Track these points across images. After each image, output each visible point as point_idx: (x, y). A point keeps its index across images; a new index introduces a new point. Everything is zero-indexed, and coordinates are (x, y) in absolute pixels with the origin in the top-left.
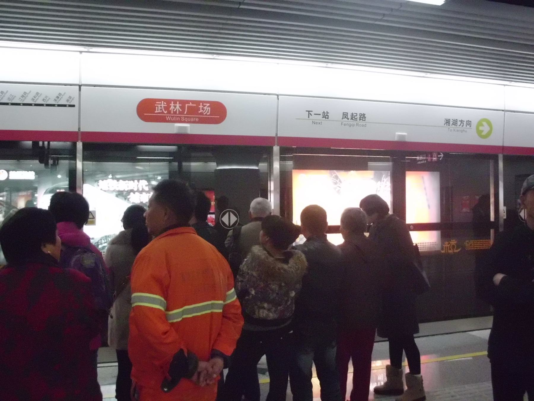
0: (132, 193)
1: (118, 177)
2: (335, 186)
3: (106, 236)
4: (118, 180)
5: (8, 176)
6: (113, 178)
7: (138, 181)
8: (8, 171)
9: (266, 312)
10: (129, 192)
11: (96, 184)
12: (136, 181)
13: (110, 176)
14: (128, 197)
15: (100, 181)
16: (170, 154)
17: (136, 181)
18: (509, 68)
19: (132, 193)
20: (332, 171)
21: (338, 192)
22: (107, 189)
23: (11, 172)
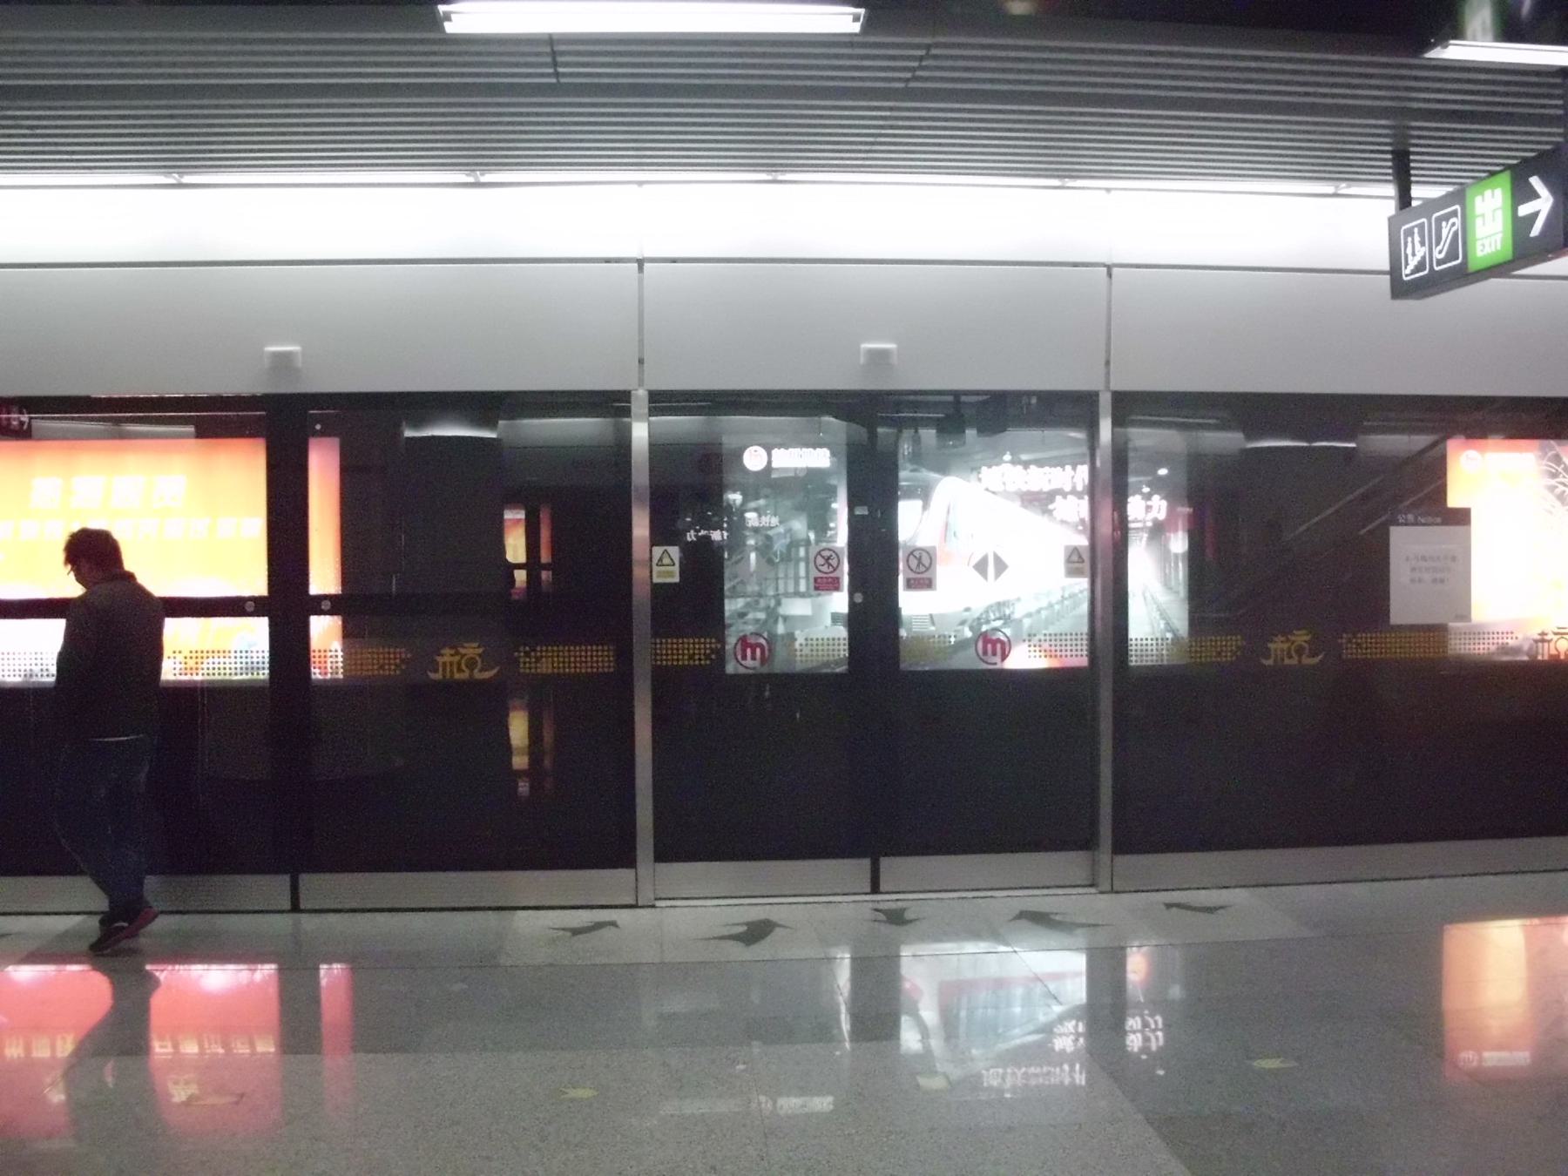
0: (1058, 498)
1: (1024, 457)
2: (1553, 482)
3: (999, 604)
4: (1026, 465)
5: (769, 462)
6: (1013, 462)
7: (1074, 469)
8: (769, 449)
9: (983, 996)
10: (1051, 496)
11: (973, 476)
12: (1068, 468)
13: (1007, 457)
14: (1051, 507)
15: (984, 469)
16: (938, 419)
17: (1068, 468)
18: (1112, 133)
19: (1058, 498)
20: (1546, 442)
21: (1018, 599)
22: (1000, 488)
23: (775, 452)
